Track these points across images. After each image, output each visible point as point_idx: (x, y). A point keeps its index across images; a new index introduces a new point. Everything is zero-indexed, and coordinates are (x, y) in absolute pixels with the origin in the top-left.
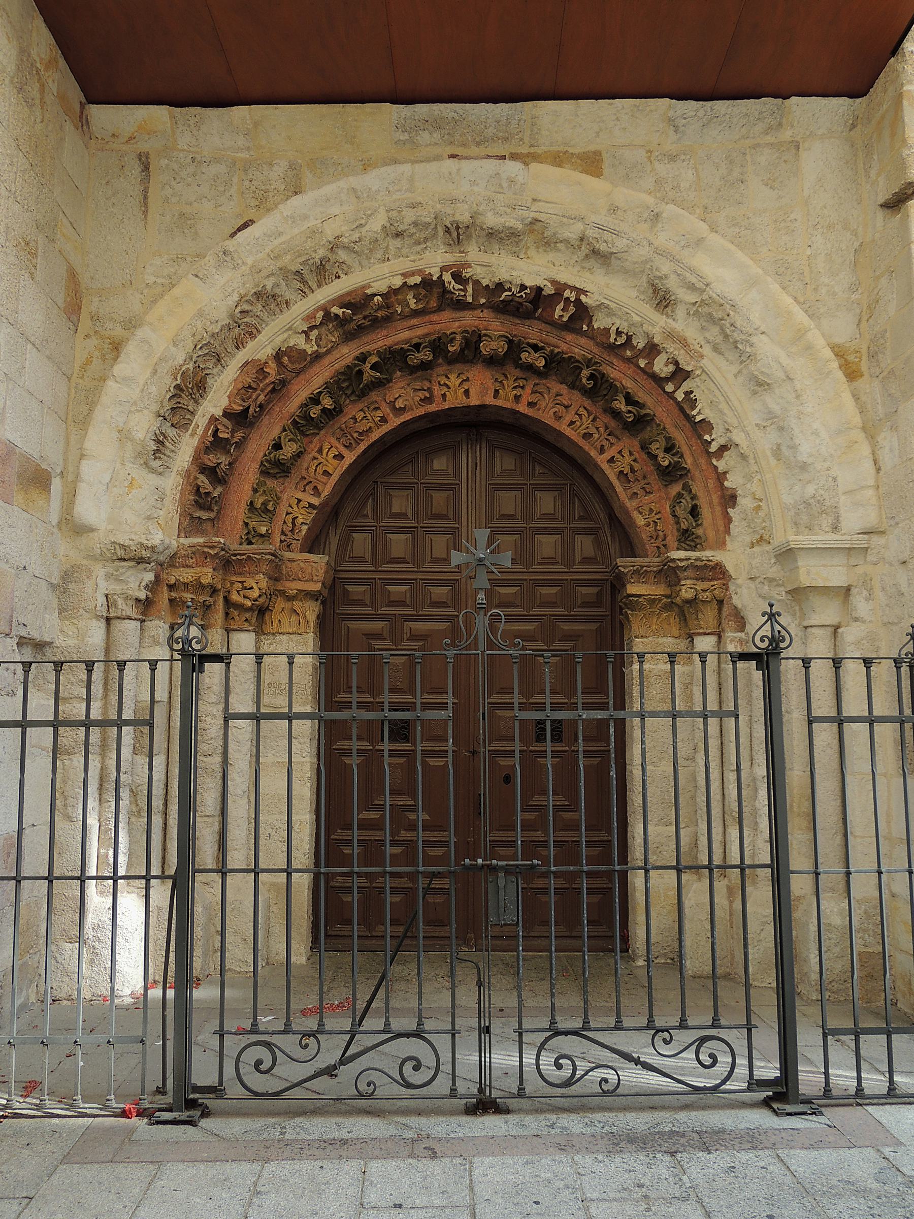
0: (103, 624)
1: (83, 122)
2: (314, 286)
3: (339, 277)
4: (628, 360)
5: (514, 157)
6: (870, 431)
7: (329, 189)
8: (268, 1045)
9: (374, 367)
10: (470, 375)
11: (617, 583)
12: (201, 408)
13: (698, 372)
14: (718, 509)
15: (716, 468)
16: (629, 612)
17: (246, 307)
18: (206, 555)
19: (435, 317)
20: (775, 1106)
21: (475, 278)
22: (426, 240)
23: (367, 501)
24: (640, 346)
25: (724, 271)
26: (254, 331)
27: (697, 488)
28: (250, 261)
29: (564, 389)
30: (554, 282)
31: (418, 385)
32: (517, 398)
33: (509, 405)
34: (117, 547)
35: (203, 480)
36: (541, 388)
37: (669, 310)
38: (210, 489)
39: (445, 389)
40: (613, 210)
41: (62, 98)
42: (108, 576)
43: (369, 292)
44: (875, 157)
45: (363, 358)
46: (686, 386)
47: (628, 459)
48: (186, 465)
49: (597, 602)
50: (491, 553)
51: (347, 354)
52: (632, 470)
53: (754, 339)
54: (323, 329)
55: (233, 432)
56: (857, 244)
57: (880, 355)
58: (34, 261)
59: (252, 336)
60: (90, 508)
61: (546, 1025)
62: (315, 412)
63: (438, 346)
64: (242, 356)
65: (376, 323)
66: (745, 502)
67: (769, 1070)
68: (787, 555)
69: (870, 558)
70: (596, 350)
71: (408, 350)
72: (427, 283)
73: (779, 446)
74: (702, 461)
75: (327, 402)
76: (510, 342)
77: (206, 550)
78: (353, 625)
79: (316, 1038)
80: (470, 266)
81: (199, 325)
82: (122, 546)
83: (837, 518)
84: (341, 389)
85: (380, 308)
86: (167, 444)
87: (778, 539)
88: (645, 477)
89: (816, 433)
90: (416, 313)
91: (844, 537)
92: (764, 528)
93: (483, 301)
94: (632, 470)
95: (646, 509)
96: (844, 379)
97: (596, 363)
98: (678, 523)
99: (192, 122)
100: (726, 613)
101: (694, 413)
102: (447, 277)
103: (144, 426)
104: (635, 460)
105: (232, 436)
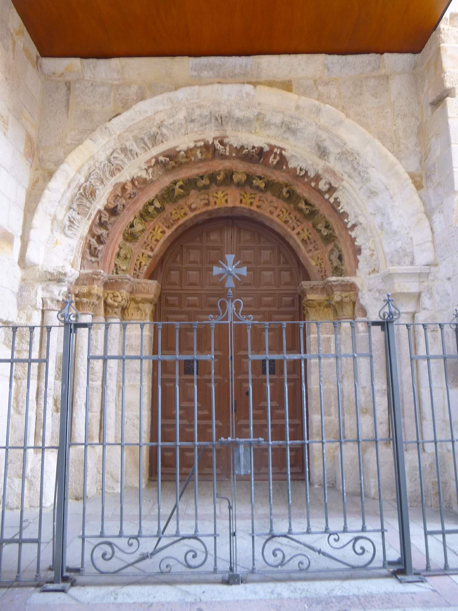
1: (38, 66)
2: (150, 146)
3: (162, 142)
4: (305, 184)
5: (249, 83)
6: (429, 214)
7: (159, 98)
8: (110, 544)
9: (181, 187)
10: (228, 192)
11: (301, 296)
12: (93, 206)
13: (341, 188)
14: (352, 257)
15: (351, 236)
16: (308, 308)
17: (115, 155)
18: (94, 279)
19: (210, 163)
20: (399, 577)
21: (230, 143)
22: (206, 124)
23: (177, 255)
24: (312, 176)
25: (353, 135)
26: (120, 168)
27: (341, 246)
28: (118, 133)
29: (274, 199)
30: (269, 145)
31: (202, 197)
32: (251, 204)
33: (247, 206)
35: (94, 241)
36: (263, 199)
37: (326, 157)
38: (97, 246)
39: (215, 199)
40: (298, 107)
41: (26, 50)
42: (43, 289)
43: (178, 149)
44: (427, 81)
45: (175, 183)
46: (335, 195)
47: (306, 233)
49: (293, 304)
50: (236, 267)
51: (167, 181)
52: (309, 238)
53: (369, 170)
54: (155, 168)
55: (109, 218)
56: (418, 124)
57: (432, 177)
58: (6, 127)
60: (34, 255)
61: (268, 531)
62: (151, 209)
63: (212, 177)
65: (180, 165)
66: (365, 252)
67: (394, 554)
68: (389, 277)
69: (431, 278)
70: (290, 179)
71: (197, 179)
73: (382, 224)
74: (343, 233)
75: (157, 205)
76: (248, 175)
77: (94, 276)
79: (138, 540)
80: (227, 137)
82: (50, 273)
83: (413, 259)
84: (164, 198)
85: (183, 157)
86: (75, 222)
87: (383, 270)
88: (315, 242)
89: (401, 216)
90: (201, 161)
91: (417, 267)
92: (375, 265)
93: (234, 155)
94: (309, 238)
95: (312, 259)
96: (414, 188)
97: (290, 185)
98: (332, 264)
100: (356, 307)
101: (339, 208)
102: (216, 142)
103: (62, 215)
104: (310, 234)
105: (109, 220)
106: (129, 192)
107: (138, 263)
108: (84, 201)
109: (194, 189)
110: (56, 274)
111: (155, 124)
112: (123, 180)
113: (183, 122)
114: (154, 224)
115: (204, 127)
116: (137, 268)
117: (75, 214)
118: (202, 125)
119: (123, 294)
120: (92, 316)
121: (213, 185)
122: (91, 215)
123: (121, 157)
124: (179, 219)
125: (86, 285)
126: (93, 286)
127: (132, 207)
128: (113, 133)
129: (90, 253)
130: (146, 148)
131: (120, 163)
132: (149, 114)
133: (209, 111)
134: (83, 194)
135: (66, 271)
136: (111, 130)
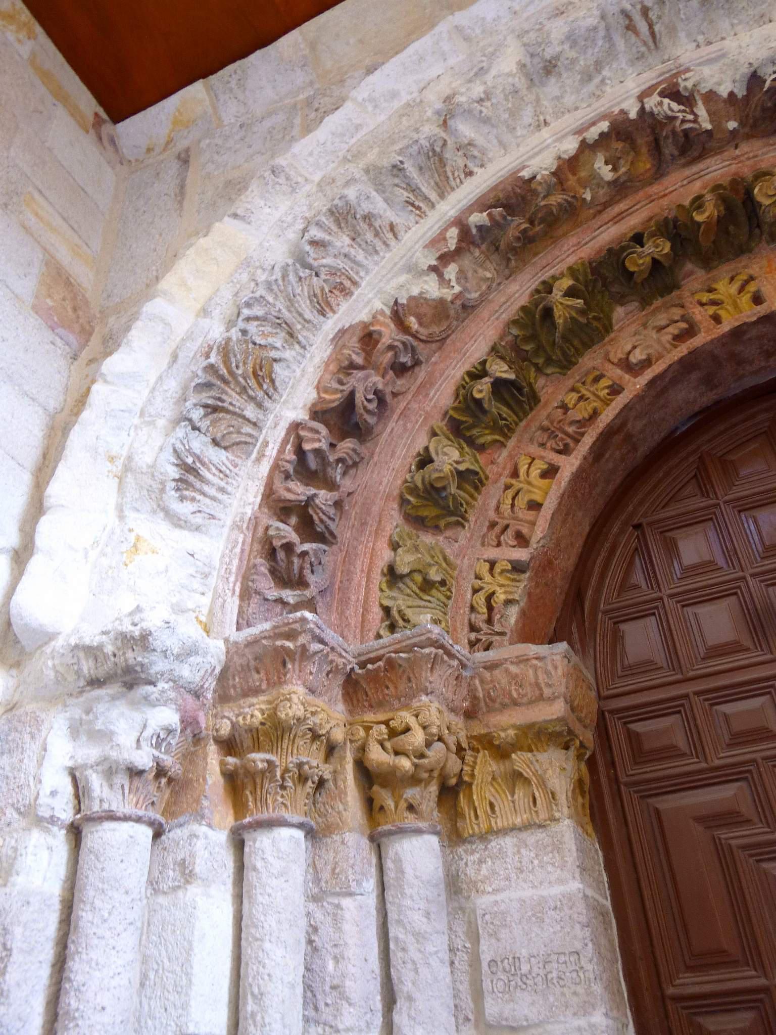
0: (59, 840)
2: (433, 196)
3: (470, 174)
9: (571, 293)
10: (754, 270)
12: (271, 417)
19: (655, 189)
22: (598, 66)
23: (631, 563)
26: (347, 284)
31: (661, 319)
34: (81, 655)
35: (287, 532)
39: (711, 310)
42: (75, 730)
45: (547, 287)
48: (249, 511)
51: (518, 292)
54: (467, 261)
59: (345, 292)
62: (482, 390)
63: (678, 230)
64: (331, 325)
72: (623, 134)
78: (667, 803)
81: (245, 277)
86: (204, 472)
99: (233, 84)
103: (154, 449)
106: (386, 341)
107: (481, 598)
108: (233, 399)
109: (621, 300)
110: (109, 649)
111: (429, 113)
112: (364, 316)
113: (520, 82)
114: (511, 457)
115: (597, 80)
116: (480, 619)
117: (199, 444)
118: (587, 77)
119: (429, 713)
120: (311, 834)
121: (689, 266)
122: (266, 443)
123: (338, 244)
124: (595, 414)
125: (256, 692)
126: (286, 689)
127: (415, 406)
128: (300, 179)
129: (273, 572)
130: (417, 205)
131: (340, 263)
132: (405, 98)
133: (596, 13)
134: (224, 371)
135: (144, 625)
136: (292, 173)
